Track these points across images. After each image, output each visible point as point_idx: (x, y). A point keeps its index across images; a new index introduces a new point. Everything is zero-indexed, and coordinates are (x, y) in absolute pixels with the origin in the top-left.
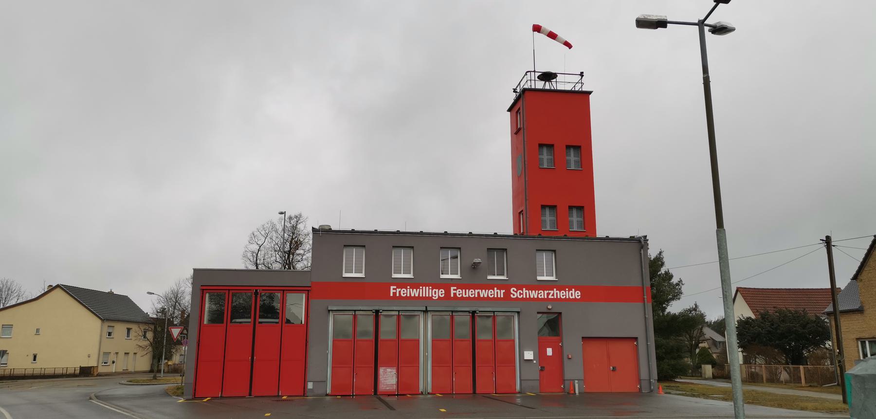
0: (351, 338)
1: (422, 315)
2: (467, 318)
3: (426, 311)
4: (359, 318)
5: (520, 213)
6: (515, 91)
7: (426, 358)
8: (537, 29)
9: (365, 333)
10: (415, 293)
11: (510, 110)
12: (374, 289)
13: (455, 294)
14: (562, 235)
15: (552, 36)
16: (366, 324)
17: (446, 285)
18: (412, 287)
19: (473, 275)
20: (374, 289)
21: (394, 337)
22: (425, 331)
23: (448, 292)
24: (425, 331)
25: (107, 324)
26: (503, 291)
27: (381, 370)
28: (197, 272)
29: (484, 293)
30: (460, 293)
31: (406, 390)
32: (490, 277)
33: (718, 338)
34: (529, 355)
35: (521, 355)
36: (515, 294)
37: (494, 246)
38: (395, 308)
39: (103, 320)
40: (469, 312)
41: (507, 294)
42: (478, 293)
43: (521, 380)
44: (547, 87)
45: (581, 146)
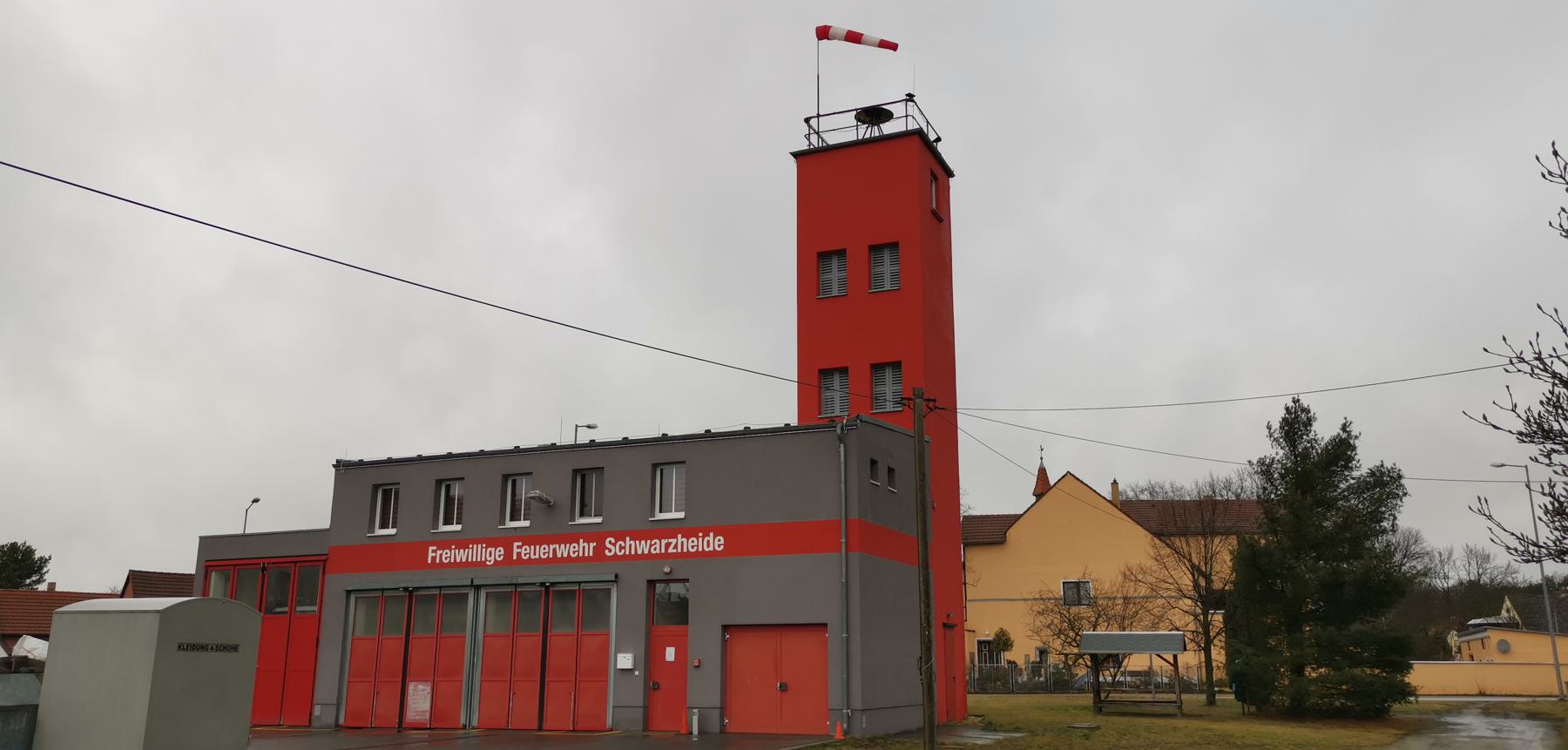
7: (472, 665)
8: (823, 33)
10: (461, 556)
13: (434, 558)
15: (854, 38)
18: (687, 536)
27: (411, 686)
28: (206, 542)
29: (563, 551)
31: (440, 722)
36: (612, 548)
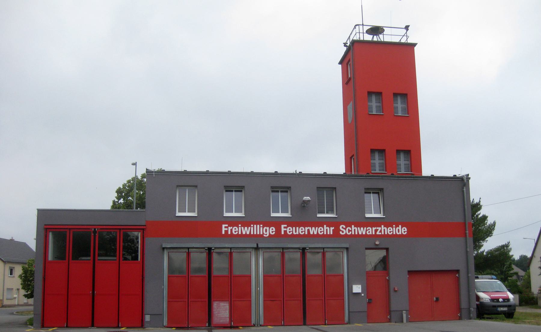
0: (185, 274)
1: (253, 252)
2: (298, 255)
3: (257, 249)
4: (192, 255)
5: (351, 158)
6: (345, 44)
7: (257, 293)
9: (199, 270)
10: (246, 231)
11: (341, 63)
12: (207, 227)
13: (285, 232)
14: (389, 174)
16: (199, 260)
17: (277, 223)
19: (303, 215)
20: (207, 227)
21: (226, 273)
22: (257, 268)
23: (278, 230)
24: (257, 268)
25: (8, 266)
26: (332, 228)
27: (215, 304)
28: (42, 214)
29: (313, 231)
30: (290, 230)
32: (319, 215)
33: (521, 273)
34: (357, 289)
35: (350, 289)
36: (344, 231)
37: (324, 185)
38: (227, 246)
39: (4, 262)
40: (299, 248)
41: (337, 231)
42: (308, 230)
43: (349, 312)
44: (375, 39)
45: (408, 94)
